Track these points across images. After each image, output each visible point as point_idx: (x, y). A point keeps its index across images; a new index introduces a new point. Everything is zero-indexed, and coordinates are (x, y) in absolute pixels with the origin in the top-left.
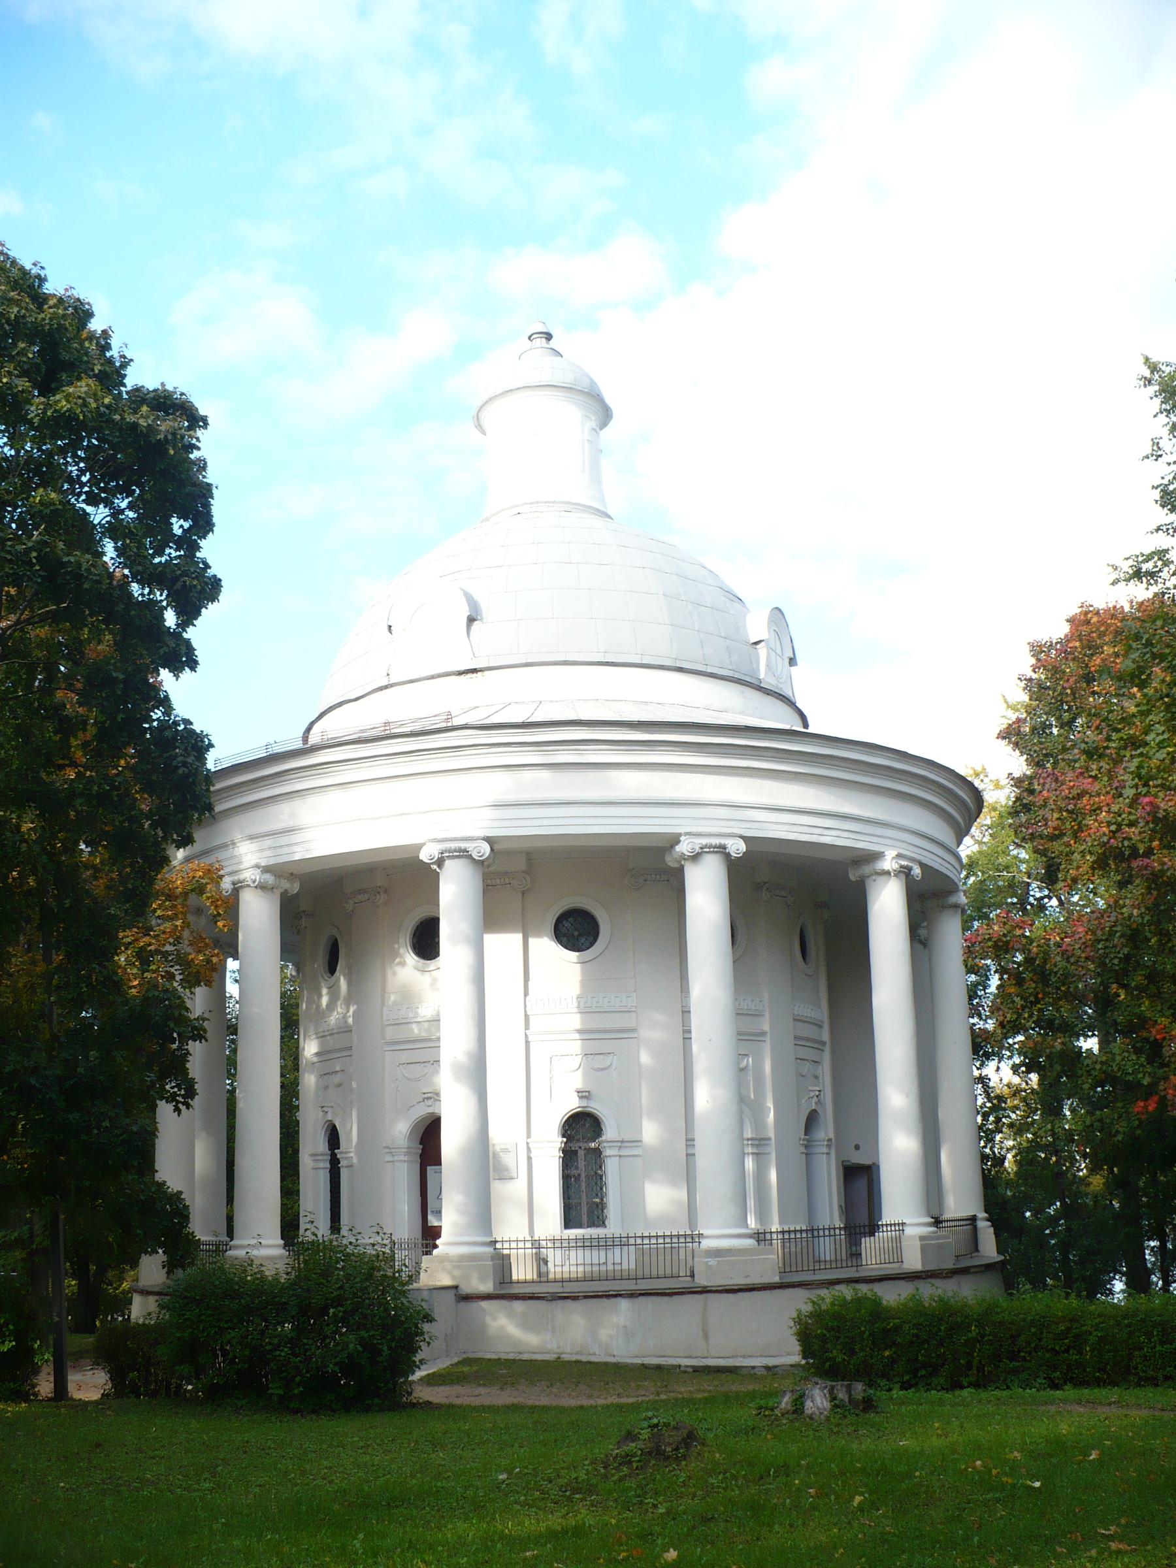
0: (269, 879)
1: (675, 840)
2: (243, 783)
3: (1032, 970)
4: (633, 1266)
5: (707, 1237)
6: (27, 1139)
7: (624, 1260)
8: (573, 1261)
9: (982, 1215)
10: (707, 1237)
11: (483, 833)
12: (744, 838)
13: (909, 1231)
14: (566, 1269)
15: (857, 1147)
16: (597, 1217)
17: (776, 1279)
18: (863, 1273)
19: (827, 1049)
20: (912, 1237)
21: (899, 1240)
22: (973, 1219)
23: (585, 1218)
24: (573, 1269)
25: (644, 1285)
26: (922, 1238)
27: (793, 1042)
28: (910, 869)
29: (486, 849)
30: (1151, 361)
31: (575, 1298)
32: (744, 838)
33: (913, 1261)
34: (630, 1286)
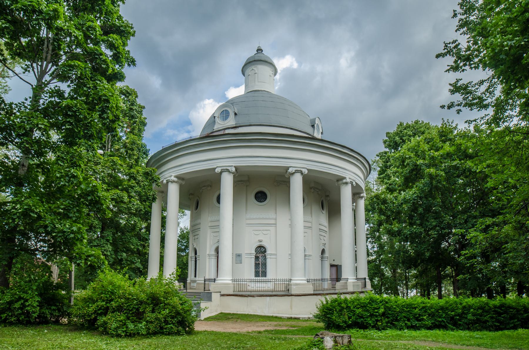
0: (176, 179)
1: (288, 168)
2: (184, 147)
3: (76, 46)
4: (273, 288)
5: (293, 280)
6: (392, 255)
7: (269, 286)
8: (256, 286)
9: (367, 278)
10: (293, 280)
11: (234, 165)
12: (308, 169)
13: (349, 281)
14: (254, 288)
15: (334, 260)
16: (264, 274)
17: (312, 292)
18: (337, 291)
19: (328, 233)
20: (350, 283)
21: (346, 283)
22: (365, 279)
23: (260, 275)
24: (256, 288)
25: (274, 293)
26: (353, 283)
27: (303, 227)
28: (353, 183)
29: (234, 170)
30: (441, 57)
31: (253, 296)
32: (308, 169)
33: (350, 289)
34: (271, 293)
